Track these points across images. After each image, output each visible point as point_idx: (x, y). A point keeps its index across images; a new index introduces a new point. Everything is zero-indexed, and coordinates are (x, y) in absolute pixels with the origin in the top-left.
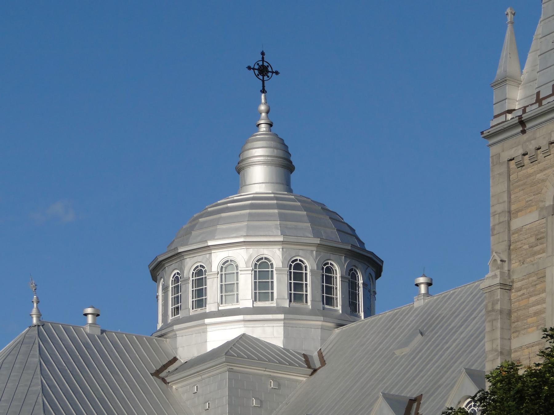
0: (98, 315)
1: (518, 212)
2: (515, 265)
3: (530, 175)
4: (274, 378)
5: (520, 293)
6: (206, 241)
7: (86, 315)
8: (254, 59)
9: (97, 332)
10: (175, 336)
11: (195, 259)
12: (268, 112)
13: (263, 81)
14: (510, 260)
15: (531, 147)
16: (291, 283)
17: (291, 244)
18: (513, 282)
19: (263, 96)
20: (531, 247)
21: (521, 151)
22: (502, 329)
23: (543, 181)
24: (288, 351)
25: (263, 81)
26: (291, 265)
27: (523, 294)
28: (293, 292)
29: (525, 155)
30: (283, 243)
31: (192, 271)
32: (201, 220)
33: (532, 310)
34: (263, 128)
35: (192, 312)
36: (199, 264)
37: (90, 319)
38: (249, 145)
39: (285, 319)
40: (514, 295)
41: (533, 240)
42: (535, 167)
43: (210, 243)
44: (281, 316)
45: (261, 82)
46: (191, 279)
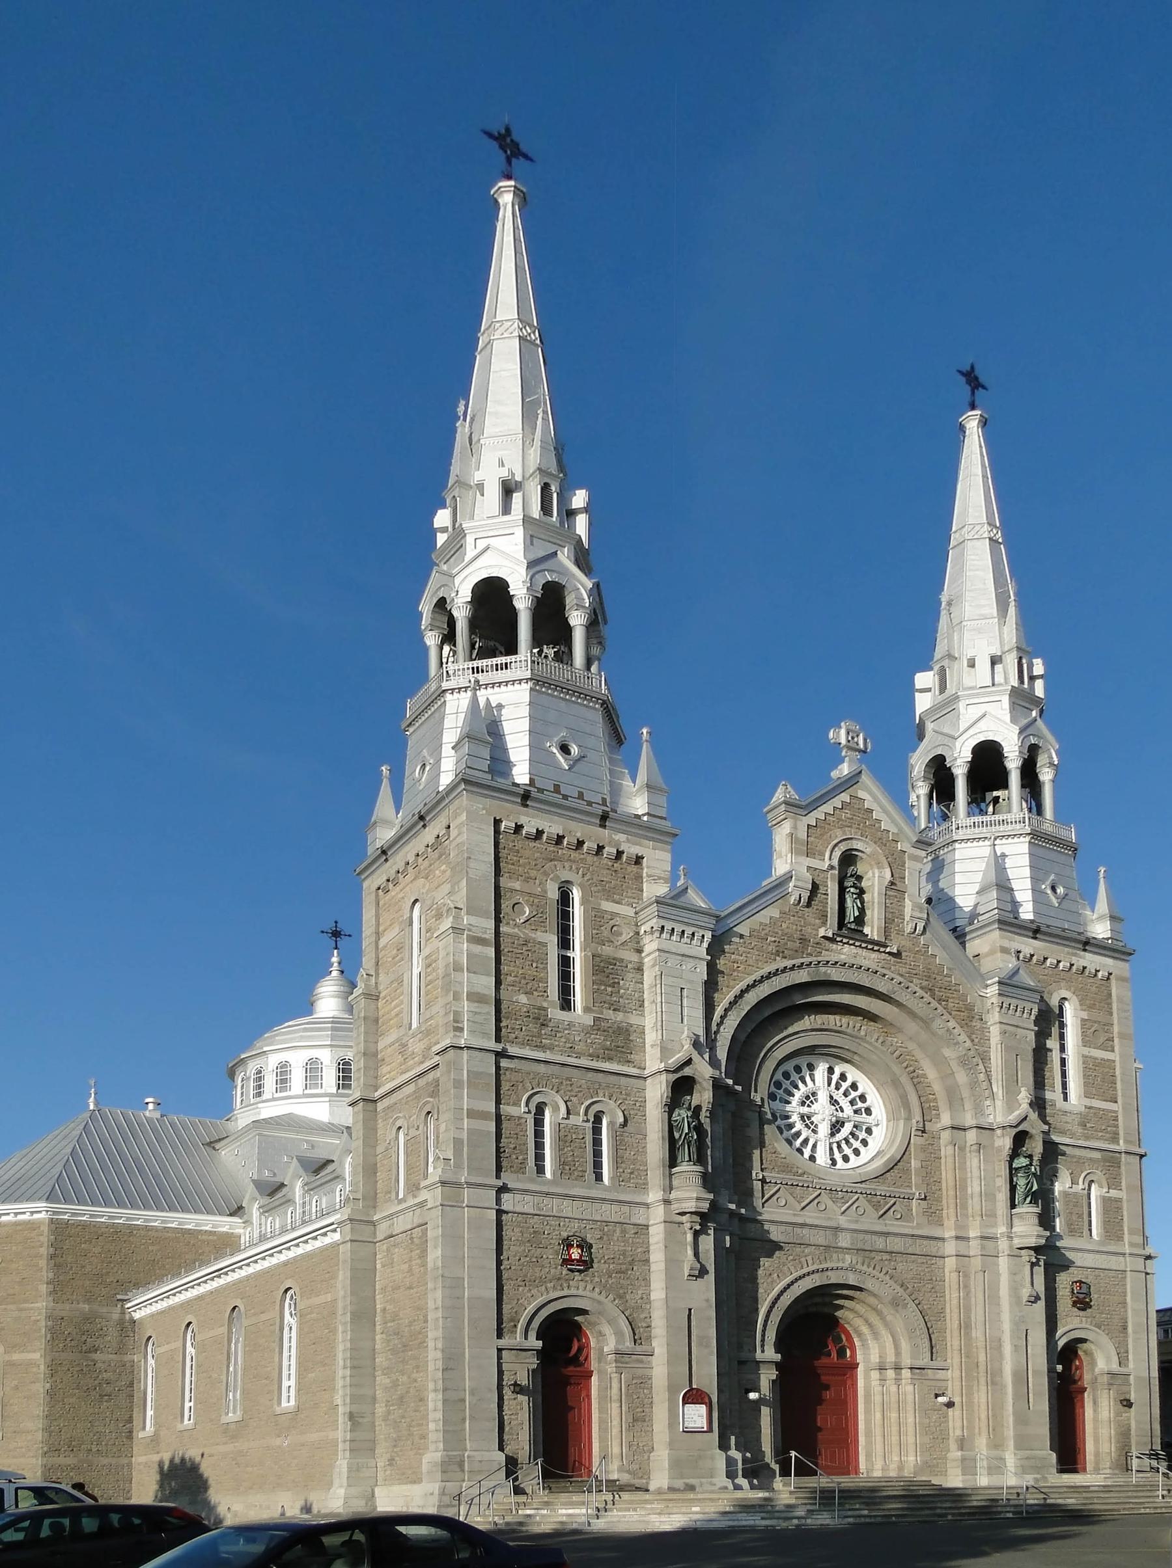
0: (159, 1104)
1: (384, 931)
2: (382, 977)
3: (393, 897)
4: (307, 1141)
5: (384, 1001)
6: (262, 1048)
7: (147, 1103)
8: (329, 926)
9: (157, 1115)
10: (237, 1118)
11: (256, 1063)
12: (339, 963)
13: (336, 941)
14: (377, 974)
15: (393, 872)
16: (339, 1076)
17: (309, 1036)
18: (380, 993)
19: (336, 951)
20: (393, 959)
21: (385, 878)
22: (366, 1033)
23: (403, 898)
24: (333, 1124)
25: (336, 941)
26: (339, 1063)
27: (387, 1001)
28: (341, 1082)
29: (388, 880)
30: (331, 1046)
31: (253, 1071)
32: (277, 1038)
33: (393, 1013)
34: (335, 974)
35: (252, 1101)
36: (259, 1066)
37: (151, 1106)
38: (319, 984)
39: (330, 1101)
40: (381, 1003)
41: (395, 951)
42: (398, 888)
43: (265, 1049)
44: (327, 1099)
45: (334, 943)
46: (253, 1077)
